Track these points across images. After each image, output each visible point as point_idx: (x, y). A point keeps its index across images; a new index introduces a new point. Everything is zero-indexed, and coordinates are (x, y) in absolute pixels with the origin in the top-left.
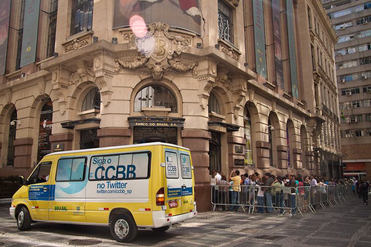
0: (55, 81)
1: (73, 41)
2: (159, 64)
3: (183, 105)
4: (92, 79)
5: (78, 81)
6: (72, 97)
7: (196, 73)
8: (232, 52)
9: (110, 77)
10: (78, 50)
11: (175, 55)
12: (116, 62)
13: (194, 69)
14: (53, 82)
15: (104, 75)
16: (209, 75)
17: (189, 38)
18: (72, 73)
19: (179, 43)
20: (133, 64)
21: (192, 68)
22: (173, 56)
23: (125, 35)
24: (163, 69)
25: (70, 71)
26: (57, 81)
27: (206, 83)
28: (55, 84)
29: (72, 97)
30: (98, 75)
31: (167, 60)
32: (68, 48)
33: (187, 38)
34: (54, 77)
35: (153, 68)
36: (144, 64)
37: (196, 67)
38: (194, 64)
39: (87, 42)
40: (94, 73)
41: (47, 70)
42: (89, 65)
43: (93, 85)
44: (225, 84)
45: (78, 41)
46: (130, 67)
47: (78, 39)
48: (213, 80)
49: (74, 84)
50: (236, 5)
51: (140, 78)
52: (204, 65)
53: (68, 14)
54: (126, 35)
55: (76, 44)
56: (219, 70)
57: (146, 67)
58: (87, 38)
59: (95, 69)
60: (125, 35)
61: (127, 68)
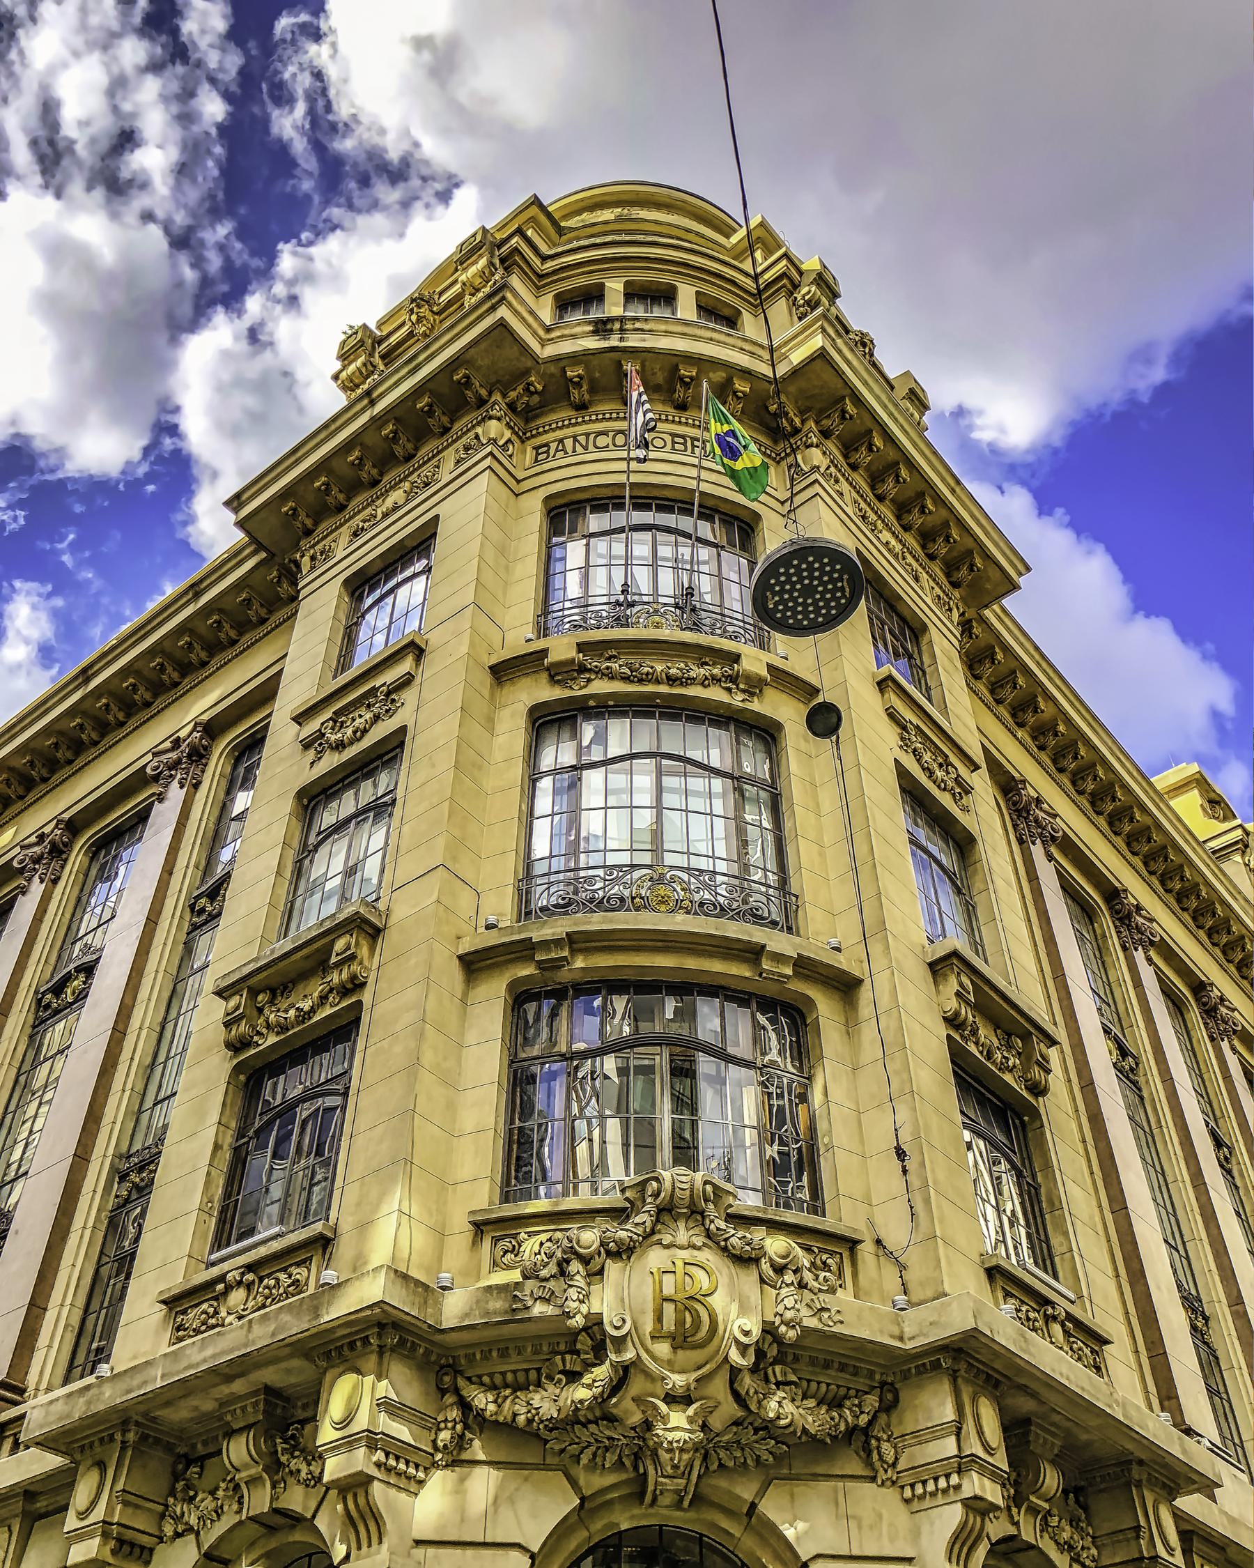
0: (82, 1515)
1: (222, 1278)
2: (685, 1400)
3: (590, 1493)
4: (296, 1499)
5: (219, 1512)
6: (685, 776)
7: (888, 1451)
8: (1067, 1333)
9: (403, 1483)
10: (245, 1328)
11: (776, 1353)
12: (443, 1392)
13: (876, 1431)
14: (71, 1522)
15: (374, 1472)
16: (963, 1464)
17: (832, 1253)
18: (189, 1461)
19: (789, 1277)
20: (537, 1399)
21: (863, 1420)
22: (760, 1354)
23: (496, 1240)
24: (704, 1427)
25: (182, 1450)
26: (99, 1514)
27: (951, 1516)
28: (79, 1536)
29: (685, 776)
30: (333, 1468)
31: (724, 1375)
32: (193, 1318)
33: (821, 1250)
34: (82, 1495)
35: (648, 1426)
36: (601, 1401)
37: (883, 1418)
38: (872, 1401)
39: (296, 1283)
40: (315, 1456)
41: (56, 1451)
42: (286, 1418)
43: (298, 1536)
44: (1054, 1521)
45: (250, 1277)
46: (521, 1419)
47: (250, 1268)
48: (993, 1493)
49: (190, 1529)
50: (1039, 1090)
51: (574, 1483)
52: (936, 1404)
53: (217, 1147)
54: (506, 1244)
55: (237, 1296)
56: (1016, 1430)
57: (612, 1419)
58: (298, 1264)
59: (327, 1434)
60: (496, 1240)
61: (504, 1429)
